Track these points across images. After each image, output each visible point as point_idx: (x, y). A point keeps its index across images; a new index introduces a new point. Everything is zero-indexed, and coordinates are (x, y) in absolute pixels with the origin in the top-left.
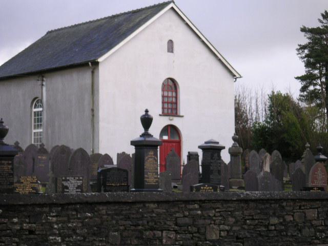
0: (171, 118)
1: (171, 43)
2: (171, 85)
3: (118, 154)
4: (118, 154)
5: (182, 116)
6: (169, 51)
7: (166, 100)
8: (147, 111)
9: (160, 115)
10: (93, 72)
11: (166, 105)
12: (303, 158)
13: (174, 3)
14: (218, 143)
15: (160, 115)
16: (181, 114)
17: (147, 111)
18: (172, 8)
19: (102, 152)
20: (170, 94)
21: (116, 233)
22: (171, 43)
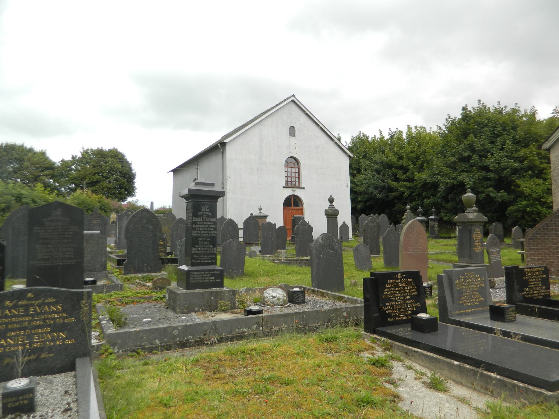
0: (294, 189)
1: (292, 128)
2: (293, 162)
3: (419, 272)
4: (419, 272)
5: (304, 188)
6: (291, 135)
7: (289, 175)
8: (331, 196)
9: (284, 187)
10: (223, 152)
11: (289, 179)
12: (404, 219)
13: (294, 96)
14: (212, 185)
15: (284, 187)
16: (303, 186)
17: (331, 196)
18: (293, 101)
19: (228, 217)
20: (293, 170)
21: (51, 180)
22: (292, 128)
